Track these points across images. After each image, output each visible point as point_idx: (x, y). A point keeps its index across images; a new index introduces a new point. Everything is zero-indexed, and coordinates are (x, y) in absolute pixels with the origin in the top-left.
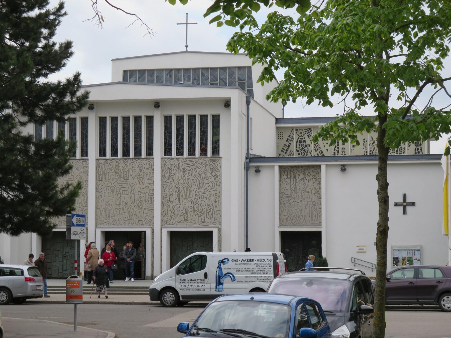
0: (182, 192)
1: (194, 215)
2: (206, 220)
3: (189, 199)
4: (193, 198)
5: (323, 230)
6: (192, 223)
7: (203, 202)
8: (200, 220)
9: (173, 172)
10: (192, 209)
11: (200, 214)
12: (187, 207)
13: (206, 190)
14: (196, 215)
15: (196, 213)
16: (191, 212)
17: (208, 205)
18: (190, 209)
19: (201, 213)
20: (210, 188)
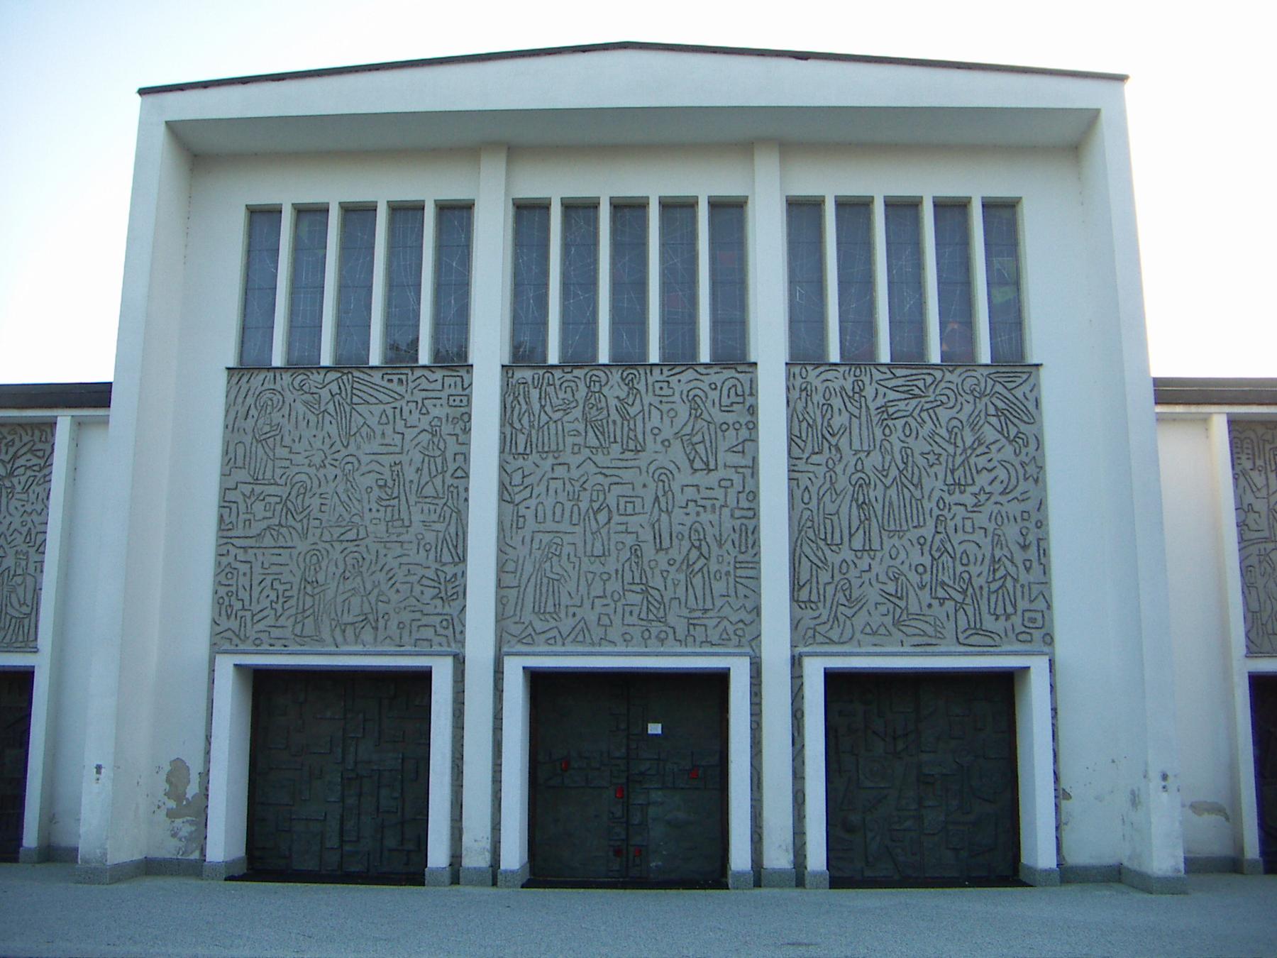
0: (878, 507)
1: (935, 603)
2: (989, 622)
3: (913, 534)
4: (928, 531)
5: (42, 663)
6: (925, 634)
7: (972, 548)
8: (962, 623)
9: (839, 421)
10: (927, 577)
11: (959, 597)
12: (905, 568)
14: (942, 601)
15: (941, 593)
16: (922, 587)
17: (994, 560)
19: (964, 592)
20: (997, 487)
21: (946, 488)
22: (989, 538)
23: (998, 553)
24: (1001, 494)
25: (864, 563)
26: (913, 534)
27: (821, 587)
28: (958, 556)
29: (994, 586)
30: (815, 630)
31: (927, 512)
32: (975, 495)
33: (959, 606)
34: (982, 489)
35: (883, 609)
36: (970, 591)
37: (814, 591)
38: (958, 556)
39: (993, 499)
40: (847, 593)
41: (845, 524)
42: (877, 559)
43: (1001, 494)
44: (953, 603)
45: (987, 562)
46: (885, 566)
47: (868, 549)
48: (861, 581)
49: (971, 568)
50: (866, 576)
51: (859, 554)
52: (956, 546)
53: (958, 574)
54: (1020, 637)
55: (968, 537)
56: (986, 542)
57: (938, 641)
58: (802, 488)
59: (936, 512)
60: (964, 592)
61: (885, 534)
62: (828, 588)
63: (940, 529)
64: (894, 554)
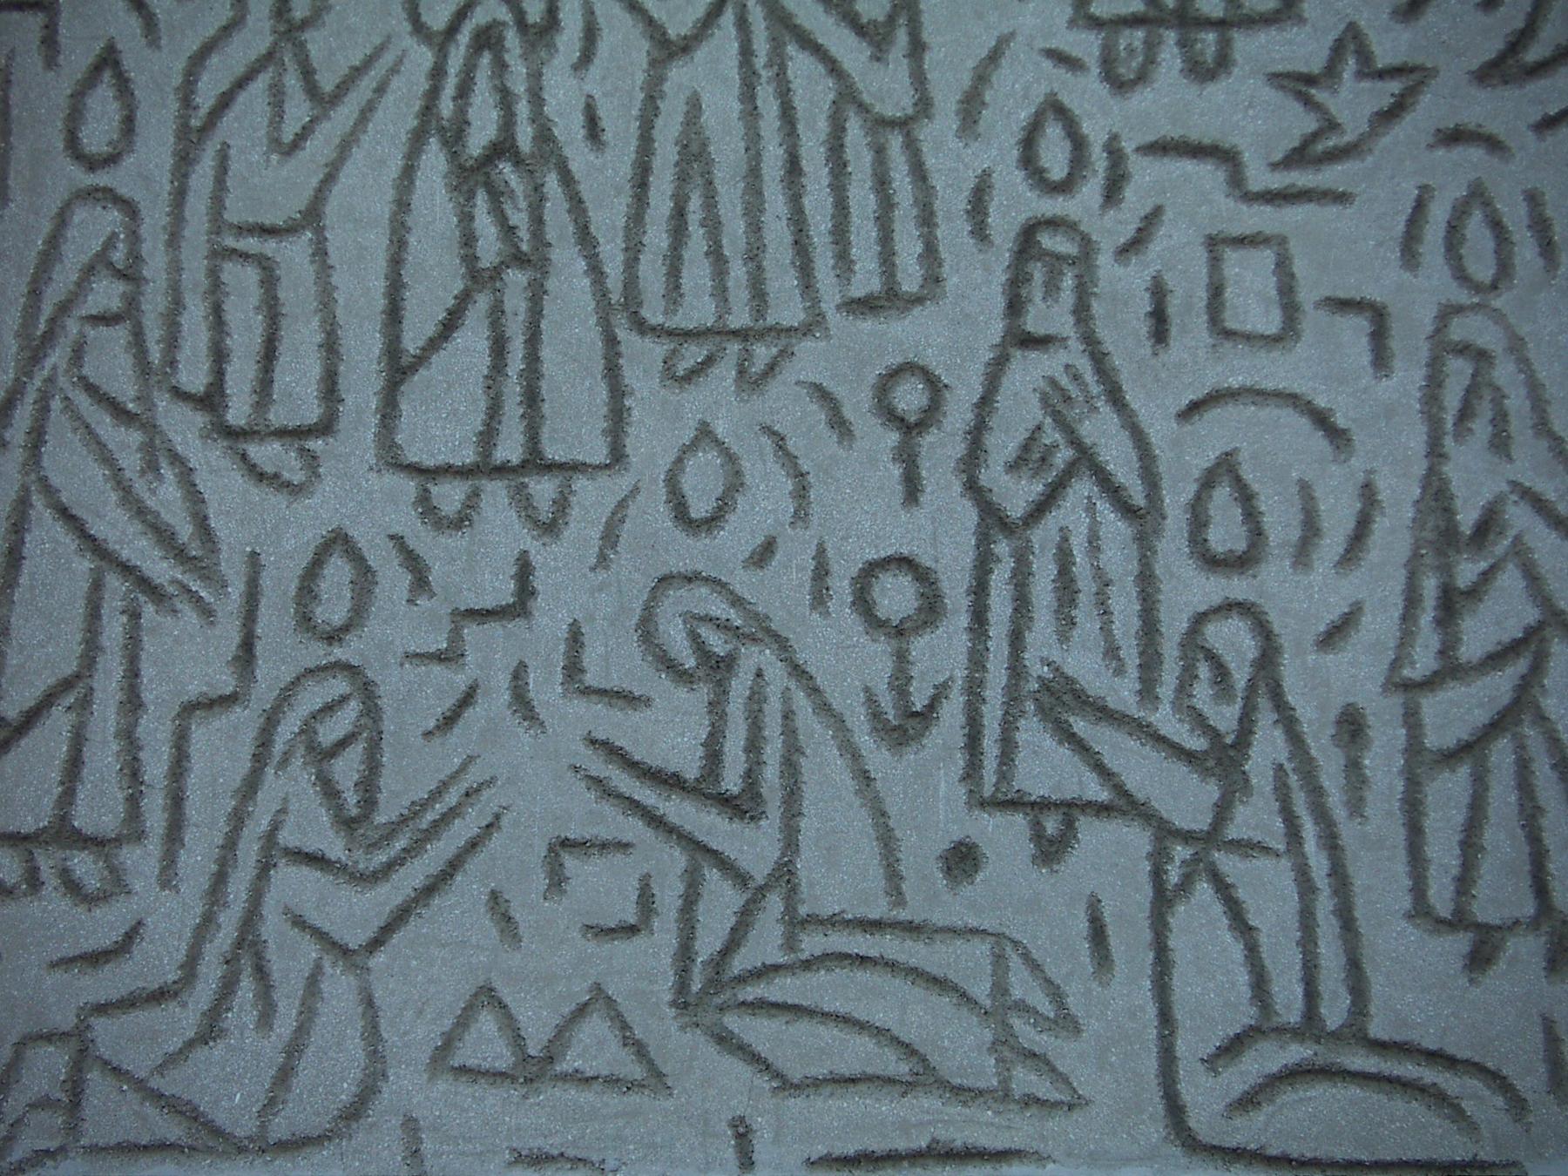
0: (603, 176)
1: (1005, 837)
3: (848, 355)
4: (953, 334)
6: (922, 1074)
7: (1277, 449)
8: (1212, 989)
10: (941, 653)
11: (1186, 798)
12: (780, 592)
13: (1353, 101)
14: (1054, 830)
15: (1046, 766)
16: (906, 725)
17: (1441, 533)
18: (849, 660)
19: (1223, 759)
21: (1087, 45)
22: (1408, 377)
23: (1474, 481)
24: (1494, 72)
25: (477, 565)
26: (848, 355)
27: (156, 730)
28: (1176, 500)
29: (1453, 713)
30: (83, 1055)
31: (952, 201)
32: (1299, 85)
33: (1188, 861)
34: (1351, 41)
35: (603, 887)
36: (1268, 747)
37: (104, 757)
38: (1176, 500)
39: (1429, 111)
40: (347, 769)
41: (360, 291)
42: (584, 526)
43: (1494, 72)
44: (1138, 839)
45: (1393, 535)
46: (631, 577)
47: (518, 465)
48: (449, 681)
49: (1271, 583)
50: (492, 652)
51: (450, 495)
52: (1160, 429)
53: (1173, 627)
54: (1483, 271)
55: (1239, 368)
56: (1388, 411)
57: (1019, 1130)
58: (78, 57)
59: (1014, 202)
60: (1223, 759)
61: (643, 359)
62: (203, 735)
63: (1050, 314)
64: (702, 483)
